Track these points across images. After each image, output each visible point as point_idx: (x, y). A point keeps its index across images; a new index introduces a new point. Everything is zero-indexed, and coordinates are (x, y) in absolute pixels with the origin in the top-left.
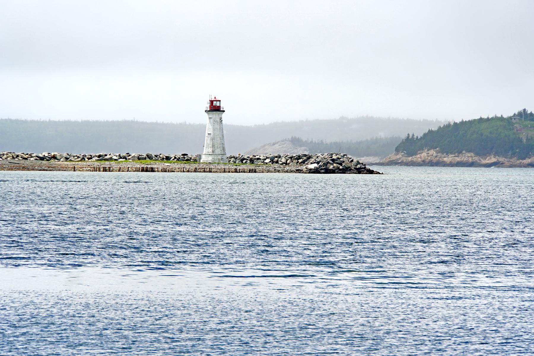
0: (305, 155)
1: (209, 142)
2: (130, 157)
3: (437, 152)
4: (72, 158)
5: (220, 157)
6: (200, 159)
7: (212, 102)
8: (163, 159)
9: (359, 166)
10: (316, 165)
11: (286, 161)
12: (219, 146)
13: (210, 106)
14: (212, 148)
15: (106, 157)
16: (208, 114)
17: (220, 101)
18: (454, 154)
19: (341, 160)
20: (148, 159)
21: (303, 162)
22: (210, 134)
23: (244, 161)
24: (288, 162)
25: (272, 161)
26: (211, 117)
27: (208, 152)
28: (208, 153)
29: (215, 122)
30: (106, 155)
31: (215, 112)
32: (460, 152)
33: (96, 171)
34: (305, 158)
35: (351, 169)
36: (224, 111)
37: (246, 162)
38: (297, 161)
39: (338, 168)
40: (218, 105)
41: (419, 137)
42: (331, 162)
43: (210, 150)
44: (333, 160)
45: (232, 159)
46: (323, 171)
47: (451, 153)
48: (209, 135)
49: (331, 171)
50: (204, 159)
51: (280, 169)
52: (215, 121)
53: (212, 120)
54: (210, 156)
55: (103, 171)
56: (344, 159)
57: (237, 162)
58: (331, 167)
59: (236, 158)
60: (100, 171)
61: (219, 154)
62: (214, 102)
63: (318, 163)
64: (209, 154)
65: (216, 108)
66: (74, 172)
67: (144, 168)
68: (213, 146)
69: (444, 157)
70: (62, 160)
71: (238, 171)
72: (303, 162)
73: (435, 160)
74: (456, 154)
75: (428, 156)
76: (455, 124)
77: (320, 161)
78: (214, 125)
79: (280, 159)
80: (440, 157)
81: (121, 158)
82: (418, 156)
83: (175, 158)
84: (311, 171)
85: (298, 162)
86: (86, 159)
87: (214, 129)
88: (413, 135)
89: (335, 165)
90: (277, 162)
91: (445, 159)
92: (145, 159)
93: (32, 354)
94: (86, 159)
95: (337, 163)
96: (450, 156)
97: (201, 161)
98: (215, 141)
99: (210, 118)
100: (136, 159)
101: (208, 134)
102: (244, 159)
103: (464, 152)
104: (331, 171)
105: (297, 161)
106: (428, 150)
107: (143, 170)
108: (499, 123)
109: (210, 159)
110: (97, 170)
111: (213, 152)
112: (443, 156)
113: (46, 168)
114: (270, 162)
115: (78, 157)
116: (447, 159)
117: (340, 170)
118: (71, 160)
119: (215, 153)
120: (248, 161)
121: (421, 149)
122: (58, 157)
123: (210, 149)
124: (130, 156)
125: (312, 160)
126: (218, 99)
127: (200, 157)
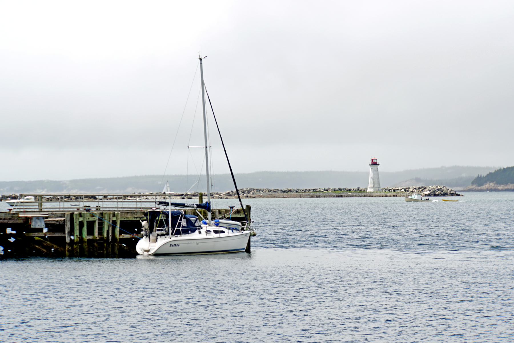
0: (423, 187)
1: (371, 181)
2: (330, 190)
3: (495, 184)
4: (299, 191)
5: (377, 189)
6: (367, 190)
7: (372, 160)
8: (347, 190)
9: (452, 192)
10: (429, 192)
13: (372, 163)
15: (317, 190)
16: (371, 166)
17: (377, 159)
18: (504, 184)
19: (442, 189)
20: (339, 191)
21: (422, 191)
23: (390, 191)
24: (414, 191)
25: (405, 190)
30: (317, 189)
32: (507, 184)
34: (423, 189)
35: (448, 194)
36: (379, 165)
37: (391, 191)
38: (418, 190)
39: (441, 194)
40: (376, 161)
41: (484, 176)
42: (437, 190)
43: (372, 185)
44: (438, 189)
45: (384, 190)
46: (433, 195)
47: (502, 184)
50: (369, 190)
51: (410, 195)
53: (373, 169)
56: (444, 189)
57: (387, 191)
58: (437, 193)
59: (386, 189)
60: (314, 197)
62: (374, 160)
63: (430, 191)
69: (499, 187)
70: (294, 192)
72: (422, 191)
73: (493, 188)
74: (505, 185)
75: (490, 186)
77: (431, 190)
79: (409, 189)
80: (496, 187)
81: (325, 190)
82: (484, 186)
83: (354, 190)
86: (307, 192)
88: (481, 175)
89: (439, 192)
90: (408, 191)
91: (499, 188)
92: (338, 190)
94: (307, 192)
95: (440, 191)
96: (502, 186)
97: (368, 191)
100: (333, 191)
102: (390, 190)
103: (509, 183)
105: (418, 190)
106: (490, 183)
107: (337, 197)
109: (372, 190)
111: (374, 186)
112: (498, 186)
113: (286, 197)
115: (303, 191)
116: (500, 188)
117: (442, 194)
118: (299, 192)
120: (393, 191)
121: (486, 182)
122: (292, 191)
124: (330, 189)
125: (426, 189)
126: (375, 158)
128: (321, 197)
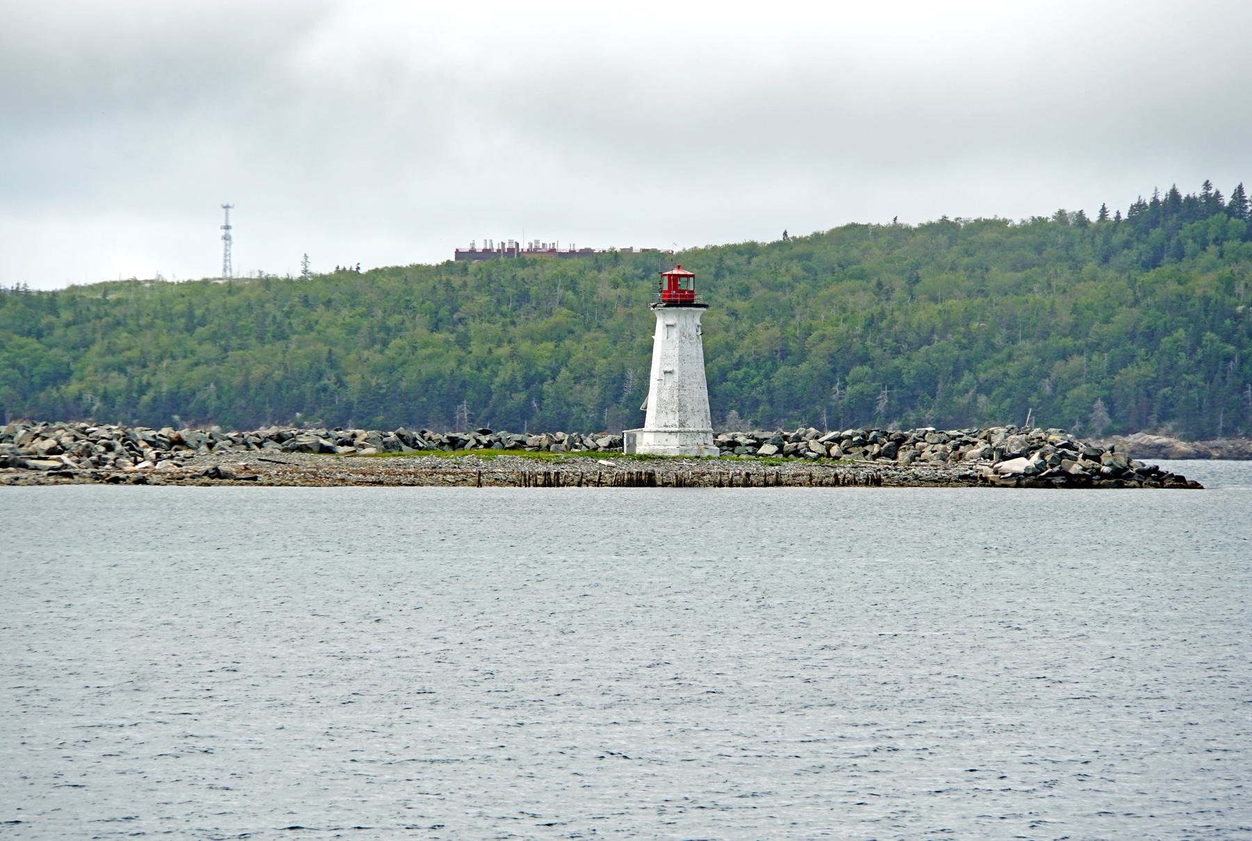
8: (442, 444)
11: (828, 450)
12: (696, 409)
14: (678, 414)
22: (670, 372)
26: (671, 322)
27: (666, 426)
28: (666, 429)
29: (685, 337)
31: (684, 309)
33: (520, 486)
43: (673, 420)
48: (668, 376)
49: (1083, 480)
52: (682, 334)
54: (673, 436)
55: (544, 485)
61: (698, 432)
64: (671, 433)
65: (685, 296)
66: (480, 489)
67: (549, 473)
68: (681, 408)
71: (841, 482)
76: (438, 266)
78: (681, 348)
84: (1019, 481)
85: (866, 453)
87: (682, 359)
93: (1109, 836)
98: (686, 393)
99: (667, 326)
101: (665, 372)
104: (1083, 480)
108: (581, 262)
109: (672, 446)
110: (531, 482)
111: (682, 424)
114: (777, 453)
117: (1104, 476)
119: (686, 429)
122: (192, 443)
123: (671, 416)
127: (631, 439)
128: (563, 486)
